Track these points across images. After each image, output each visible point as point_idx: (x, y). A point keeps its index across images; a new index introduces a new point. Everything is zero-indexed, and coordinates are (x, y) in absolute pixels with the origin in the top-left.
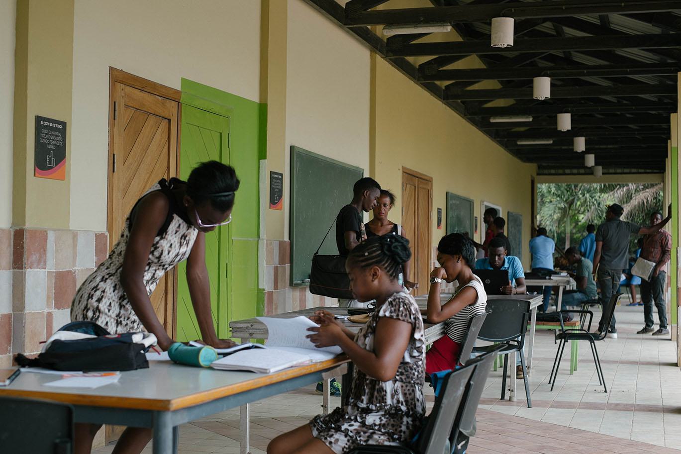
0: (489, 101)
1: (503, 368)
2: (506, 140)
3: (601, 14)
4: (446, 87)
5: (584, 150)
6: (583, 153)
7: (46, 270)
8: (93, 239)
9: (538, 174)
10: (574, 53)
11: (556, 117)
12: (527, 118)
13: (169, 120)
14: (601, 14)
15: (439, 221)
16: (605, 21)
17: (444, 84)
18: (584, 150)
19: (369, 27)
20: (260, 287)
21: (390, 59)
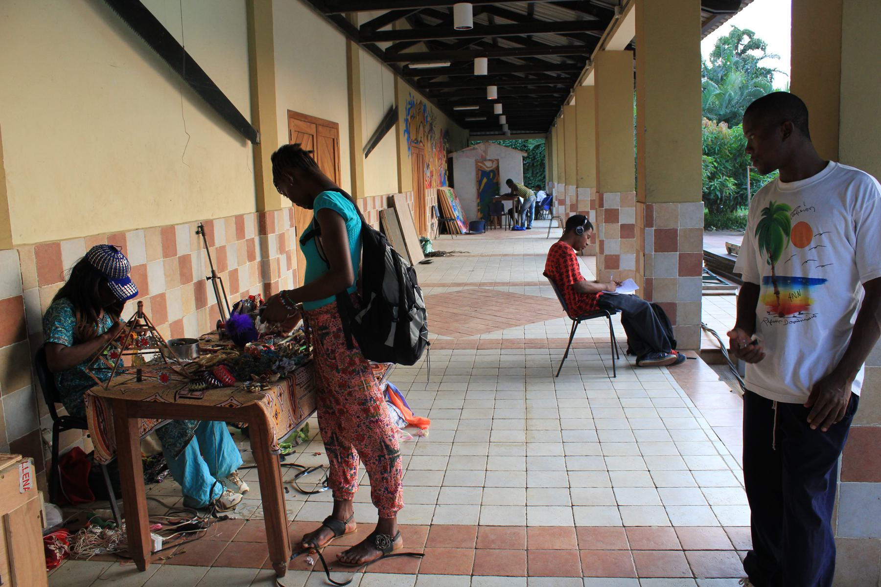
0: (434, 78)
1: (40, 518)
2: (428, 90)
3: (528, 34)
4: (418, 80)
5: (496, 98)
6: (502, 114)
7: (654, 228)
8: (315, 204)
9: (470, 135)
10: (499, 40)
11: (486, 89)
12: (476, 107)
13: (313, 136)
14: (528, 34)
15: (712, 278)
16: (529, 37)
17: (384, 45)
18: (496, 98)
19: (343, 15)
20: (557, 226)
21: (363, 45)
